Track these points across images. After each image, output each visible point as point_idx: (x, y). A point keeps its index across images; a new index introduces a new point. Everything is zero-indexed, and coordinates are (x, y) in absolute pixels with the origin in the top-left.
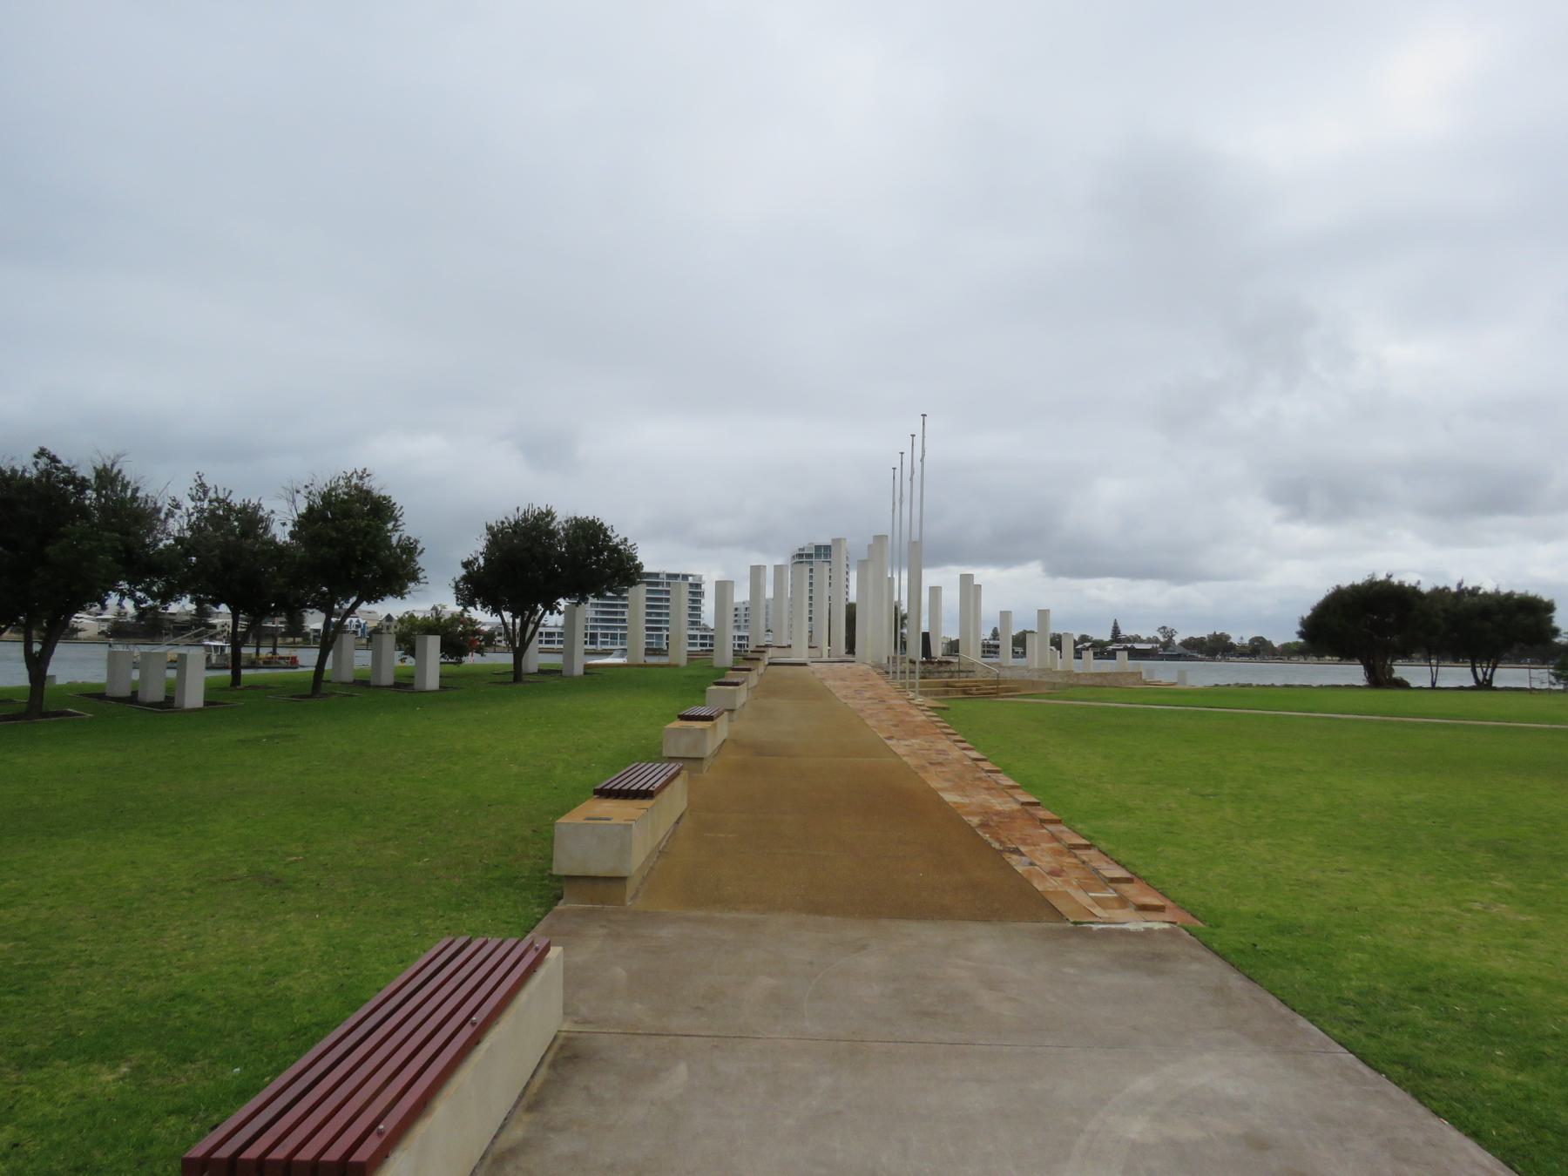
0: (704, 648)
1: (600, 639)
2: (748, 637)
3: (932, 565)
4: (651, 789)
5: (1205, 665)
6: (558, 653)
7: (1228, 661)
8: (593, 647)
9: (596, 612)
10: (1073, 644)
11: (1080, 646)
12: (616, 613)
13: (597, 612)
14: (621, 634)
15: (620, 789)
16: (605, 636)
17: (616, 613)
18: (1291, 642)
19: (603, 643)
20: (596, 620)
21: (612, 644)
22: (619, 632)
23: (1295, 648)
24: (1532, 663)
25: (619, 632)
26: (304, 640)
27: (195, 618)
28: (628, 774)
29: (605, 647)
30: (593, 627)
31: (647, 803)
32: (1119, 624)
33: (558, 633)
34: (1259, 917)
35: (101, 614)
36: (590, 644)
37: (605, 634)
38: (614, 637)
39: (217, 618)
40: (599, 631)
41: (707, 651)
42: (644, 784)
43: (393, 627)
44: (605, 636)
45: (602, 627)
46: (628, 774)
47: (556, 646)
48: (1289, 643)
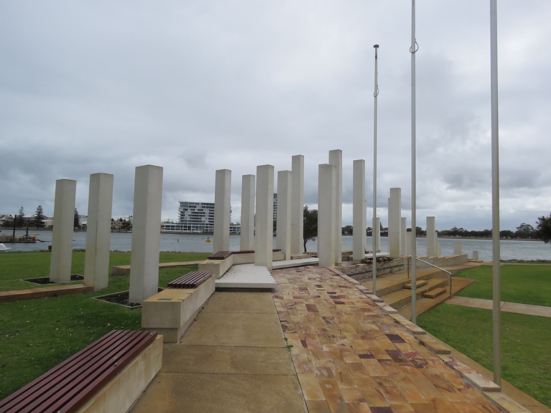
0: (231, 232)
1: (192, 228)
2: (240, 227)
3: (378, 207)
4: (195, 283)
5: (480, 242)
6: (176, 233)
7: (422, 237)
8: (189, 231)
9: (191, 218)
10: (366, 231)
11: (368, 232)
12: (198, 218)
13: (191, 218)
14: (188, 226)
15: (188, 284)
16: (194, 227)
17: (198, 218)
18: (444, 230)
19: (193, 230)
20: (190, 221)
21: (196, 230)
22: (199, 225)
23: (446, 233)
24: (531, 239)
25: (199, 225)
26: (79, 228)
27: (36, 219)
28: (182, 279)
29: (194, 231)
30: (189, 224)
31: (191, 291)
32: (381, 223)
33: (176, 226)
34: (92, 314)
35: (2, 218)
36: (188, 230)
37: (207, 227)
38: (197, 227)
39: (46, 219)
40: (192, 225)
41: (232, 233)
42: (183, 282)
43: (114, 223)
44: (194, 227)
45: (193, 224)
46: (182, 279)
47: (175, 231)
48: (444, 231)
